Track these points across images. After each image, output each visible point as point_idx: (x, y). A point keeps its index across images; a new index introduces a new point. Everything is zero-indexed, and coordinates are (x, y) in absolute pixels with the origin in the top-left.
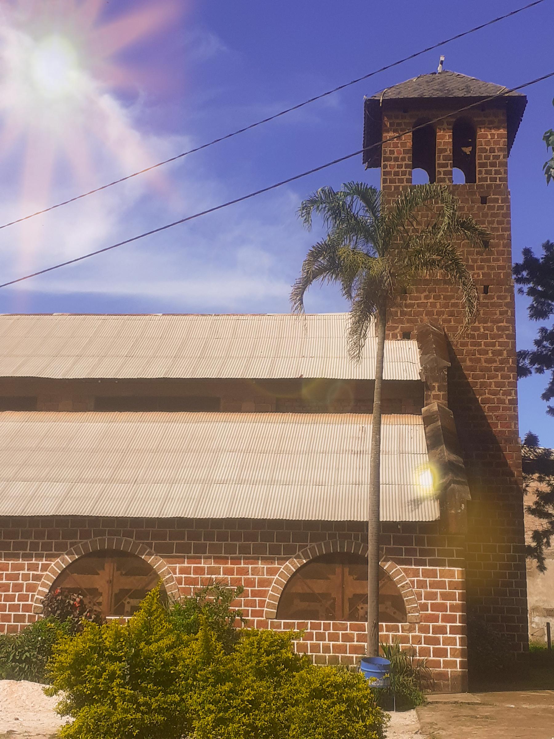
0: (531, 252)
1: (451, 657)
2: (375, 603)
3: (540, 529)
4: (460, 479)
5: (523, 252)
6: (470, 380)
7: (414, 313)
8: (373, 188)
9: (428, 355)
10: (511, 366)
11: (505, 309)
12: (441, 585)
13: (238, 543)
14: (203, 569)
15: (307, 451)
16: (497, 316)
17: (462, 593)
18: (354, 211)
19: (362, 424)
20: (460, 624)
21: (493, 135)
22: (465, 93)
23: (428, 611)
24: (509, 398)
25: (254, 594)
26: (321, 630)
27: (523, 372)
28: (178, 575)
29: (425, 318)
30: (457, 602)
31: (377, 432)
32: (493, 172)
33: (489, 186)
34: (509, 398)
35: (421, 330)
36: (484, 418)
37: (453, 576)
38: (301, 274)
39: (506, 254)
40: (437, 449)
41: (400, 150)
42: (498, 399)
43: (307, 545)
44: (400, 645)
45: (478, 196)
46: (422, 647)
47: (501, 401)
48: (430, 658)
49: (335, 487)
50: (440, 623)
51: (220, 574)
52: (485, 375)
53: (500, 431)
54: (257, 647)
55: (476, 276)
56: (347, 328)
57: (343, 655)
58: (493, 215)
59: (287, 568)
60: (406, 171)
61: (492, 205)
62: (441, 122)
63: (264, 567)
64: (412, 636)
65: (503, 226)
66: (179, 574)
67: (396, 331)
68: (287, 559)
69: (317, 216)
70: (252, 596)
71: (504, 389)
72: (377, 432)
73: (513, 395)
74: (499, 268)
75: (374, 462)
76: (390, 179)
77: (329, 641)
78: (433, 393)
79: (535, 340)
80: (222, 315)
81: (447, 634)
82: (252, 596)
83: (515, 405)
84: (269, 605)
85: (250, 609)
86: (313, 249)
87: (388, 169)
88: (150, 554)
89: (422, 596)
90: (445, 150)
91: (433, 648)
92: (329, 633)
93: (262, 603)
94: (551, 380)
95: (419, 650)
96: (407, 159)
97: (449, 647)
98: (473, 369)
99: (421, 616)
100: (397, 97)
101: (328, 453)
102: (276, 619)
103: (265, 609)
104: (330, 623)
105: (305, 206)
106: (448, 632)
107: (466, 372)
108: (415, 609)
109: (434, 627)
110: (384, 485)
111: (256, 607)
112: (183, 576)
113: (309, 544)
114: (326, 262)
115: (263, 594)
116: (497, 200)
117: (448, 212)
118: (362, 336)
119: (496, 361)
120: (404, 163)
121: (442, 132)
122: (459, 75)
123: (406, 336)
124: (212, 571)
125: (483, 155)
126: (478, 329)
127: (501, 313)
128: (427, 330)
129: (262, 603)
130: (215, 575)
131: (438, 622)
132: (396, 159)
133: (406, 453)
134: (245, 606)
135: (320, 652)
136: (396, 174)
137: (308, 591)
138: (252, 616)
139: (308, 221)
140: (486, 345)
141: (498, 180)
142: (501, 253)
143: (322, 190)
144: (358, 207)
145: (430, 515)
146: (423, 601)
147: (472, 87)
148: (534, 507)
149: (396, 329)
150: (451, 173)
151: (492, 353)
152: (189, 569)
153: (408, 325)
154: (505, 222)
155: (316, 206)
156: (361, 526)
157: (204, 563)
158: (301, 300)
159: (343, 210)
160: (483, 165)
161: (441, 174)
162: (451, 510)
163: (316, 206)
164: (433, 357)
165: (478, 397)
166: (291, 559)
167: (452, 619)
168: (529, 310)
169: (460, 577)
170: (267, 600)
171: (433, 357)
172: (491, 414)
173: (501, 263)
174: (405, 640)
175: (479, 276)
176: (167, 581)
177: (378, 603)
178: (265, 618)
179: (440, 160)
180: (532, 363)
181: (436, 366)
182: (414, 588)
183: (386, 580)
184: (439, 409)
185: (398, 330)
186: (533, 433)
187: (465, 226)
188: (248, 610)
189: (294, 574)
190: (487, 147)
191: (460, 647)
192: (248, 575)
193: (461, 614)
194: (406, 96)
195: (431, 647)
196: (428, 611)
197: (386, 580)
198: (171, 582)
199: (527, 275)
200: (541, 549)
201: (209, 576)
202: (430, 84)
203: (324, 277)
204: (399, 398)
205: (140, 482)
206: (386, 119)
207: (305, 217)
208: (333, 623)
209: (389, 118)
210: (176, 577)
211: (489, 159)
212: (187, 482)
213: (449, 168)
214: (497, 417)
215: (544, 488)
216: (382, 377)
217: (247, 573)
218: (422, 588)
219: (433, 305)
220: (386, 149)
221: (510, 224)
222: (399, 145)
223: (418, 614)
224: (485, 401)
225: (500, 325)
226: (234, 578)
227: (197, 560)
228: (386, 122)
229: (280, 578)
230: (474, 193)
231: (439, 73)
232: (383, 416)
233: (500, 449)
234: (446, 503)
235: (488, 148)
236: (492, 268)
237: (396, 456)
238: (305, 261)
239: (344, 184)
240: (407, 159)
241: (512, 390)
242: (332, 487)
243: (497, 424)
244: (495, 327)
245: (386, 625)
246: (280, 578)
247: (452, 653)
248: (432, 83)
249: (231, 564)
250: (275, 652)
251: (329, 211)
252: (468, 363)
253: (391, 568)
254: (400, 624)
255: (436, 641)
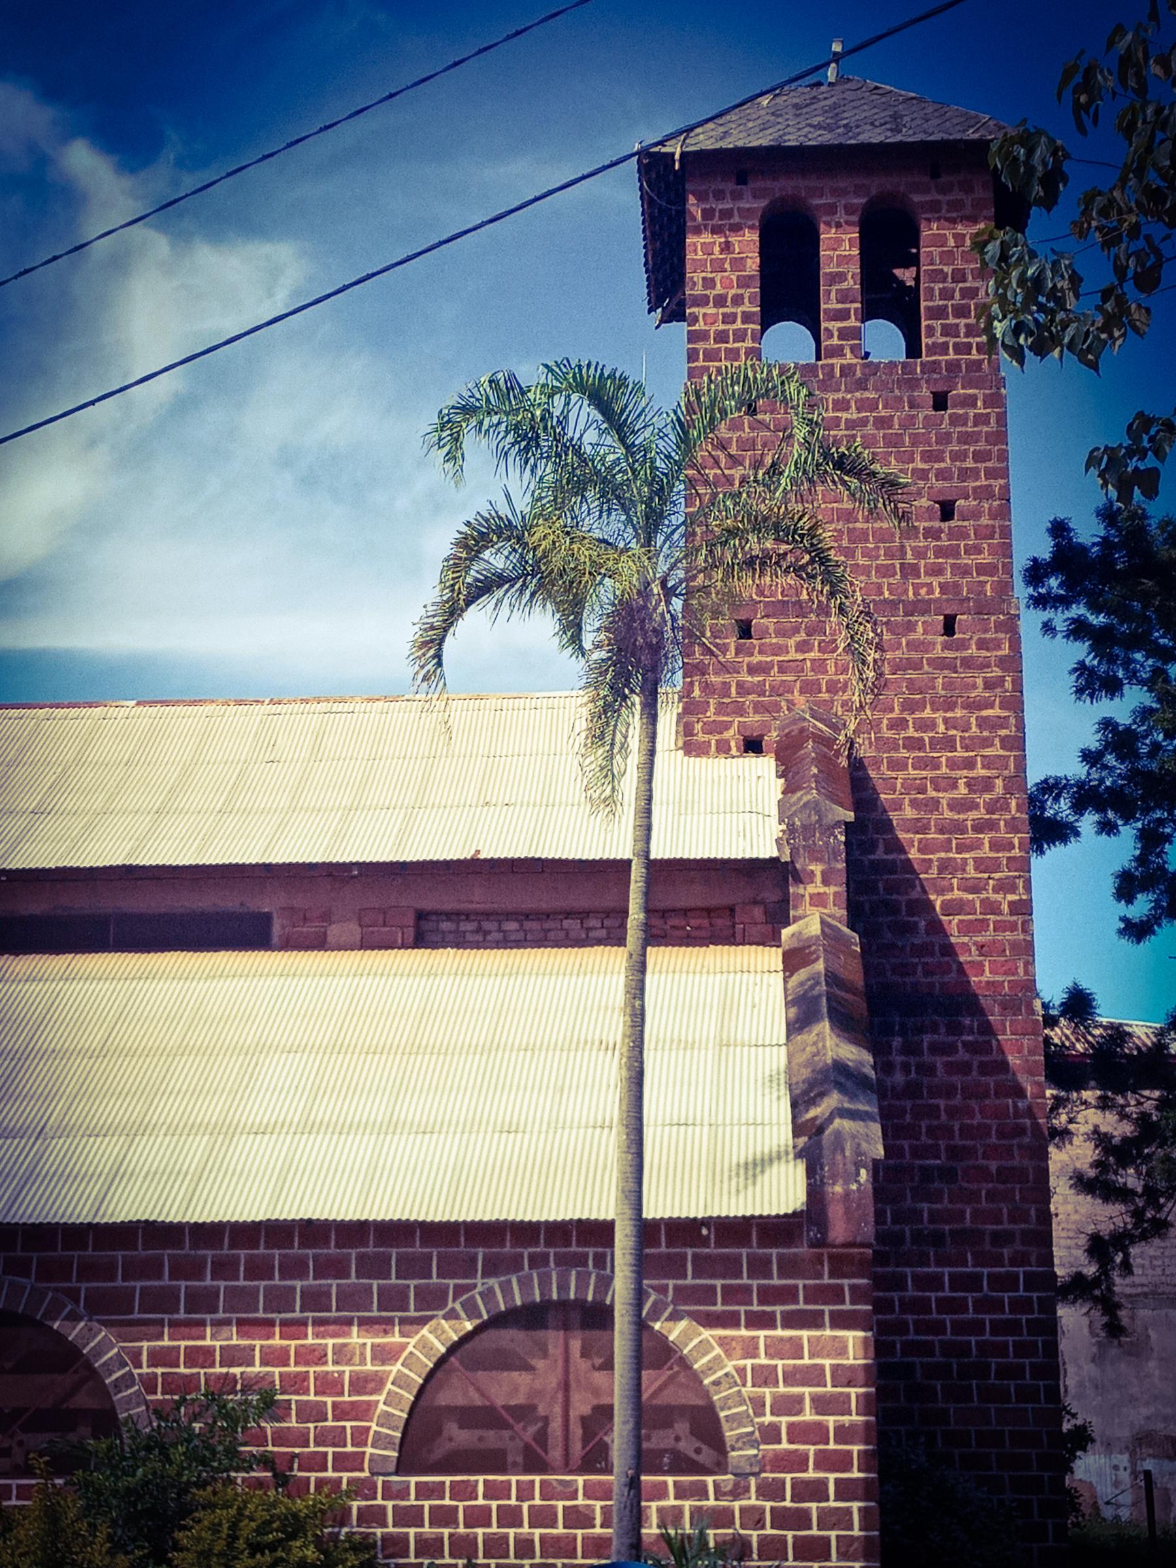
0: (1069, 530)
1: (838, 1560)
2: (630, 1426)
3: (1105, 1229)
7: (772, 688)
9: (799, 794)
10: (1014, 818)
11: (997, 672)
12: (813, 1376)
13: (298, 1284)
14: (209, 1352)
15: (487, 1047)
16: (979, 692)
17: (866, 1395)
19: (598, 971)
20: (861, 1475)
21: (959, 238)
22: (889, 134)
23: (780, 1442)
24: (1010, 897)
25: (341, 1412)
26: (509, 1498)
27: (1048, 832)
28: (145, 1370)
29: (800, 700)
30: (854, 1417)
31: (637, 990)
32: (963, 331)
33: (953, 366)
34: (1010, 897)
35: (787, 731)
36: (949, 950)
37: (842, 1352)
38: (437, 591)
39: (997, 536)
40: (810, 1032)
41: (727, 278)
42: (982, 901)
43: (475, 1286)
44: (710, 1532)
46: (767, 1536)
47: (991, 907)
48: (787, 1564)
49: (551, 1136)
50: (811, 1474)
53: (988, 982)
54: (229, 1536)
56: (577, 730)
58: (965, 438)
59: (424, 1345)
60: (746, 330)
61: (961, 412)
62: (832, 209)
63: (365, 1344)
65: (989, 464)
66: (148, 1367)
67: (727, 735)
68: (423, 1321)
69: (477, 448)
70: (336, 1418)
71: (997, 875)
72: (637, 990)
73: (1021, 890)
74: (982, 569)
75: (629, 1069)
76: (705, 349)
77: (530, 1527)
78: (811, 889)
79: (1082, 751)
80: (289, 702)
81: (827, 1500)
82: (336, 1418)
83: (1027, 917)
84: (379, 1441)
85: (330, 1450)
86: (465, 529)
87: (700, 326)
88: (74, 1317)
89: (764, 1405)
90: (841, 277)
91: (794, 1537)
92: (530, 1507)
93: (360, 1437)
94: (1138, 852)
96: (746, 300)
97: (833, 1534)
99: (764, 1457)
100: (717, 146)
101: (540, 1050)
102: (397, 1473)
103: (369, 1450)
104: (533, 1482)
105: (449, 421)
106: (832, 1496)
107: (902, 835)
108: (748, 1440)
109: (795, 1483)
110: (752, 1128)
112: (159, 1371)
113: (479, 1281)
114: (490, 565)
115: (362, 1411)
116: (971, 402)
119: (976, 807)
120: (739, 310)
121: (833, 230)
122: (876, 88)
125: (937, 287)
126: (930, 725)
127: (989, 685)
128: (802, 730)
129: (360, 1437)
130: (240, 1365)
132: (720, 301)
133: (735, 1046)
134: (317, 1444)
135: (507, 1557)
136: (722, 337)
137: (478, 1401)
138: (335, 1470)
143: (490, 382)
144: (583, 423)
145: (783, 1199)
146: (768, 1418)
147: (906, 119)
149: (727, 729)
150: (856, 334)
151: (968, 785)
152: (174, 1354)
153: (757, 718)
155: (474, 422)
156: (597, 1233)
157: (213, 1337)
158: (438, 656)
159: (545, 428)
161: (832, 336)
163: (474, 422)
164: (809, 797)
165: (932, 897)
166: (433, 1323)
167: (841, 1462)
168: (1074, 677)
169: (861, 1353)
170: (374, 1428)
171: (809, 797)
172: (966, 940)
173: (985, 558)
174: (722, 1518)
175: (931, 591)
176: (118, 1385)
177: (638, 1426)
178: (366, 1474)
179: (829, 303)
180: (1079, 807)
182: (744, 1385)
184: (822, 930)
185: (731, 732)
186: (1084, 984)
188: (326, 1454)
189: (441, 1362)
190: (945, 269)
192: (326, 1363)
193: (862, 1447)
194: (740, 144)
196: (780, 1442)
197: (676, 1368)
198: (128, 1387)
199: (1060, 586)
201: (224, 1370)
203: (499, 602)
204: (711, 902)
205: (51, 1134)
207: (447, 448)
208: (542, 1482)
209: (702, 197)
210: (139, 1375)
211: (952, 298)
213: (852, 322)
215: (1108, 1122)
217: (321, 1359)
218: (765, 1383)
219: (819, 666)
220: (695, 277)
222: (727, 266)
223: (755, 1452)
224: (952, 908)
225: (985, 713)
226: (289, 1374)
227: (195, 1331)
228: (693, 209)
229: (406, 1371)
230: (913, 384)
231: (830, 84)
232: (649, 948)
233: (987, 1029)
235: (948, 269)
236: (965, 571)
239: (546, 366)
242: (543, 1136)
243: (981, 965)
244: (973, 720)
245: (675, 1483)
246: (406, 1371)
247: (843, 1550)
249: (281, 1338)
250: (272, 1547)
252: (909, 813)
253: (686, 1336)
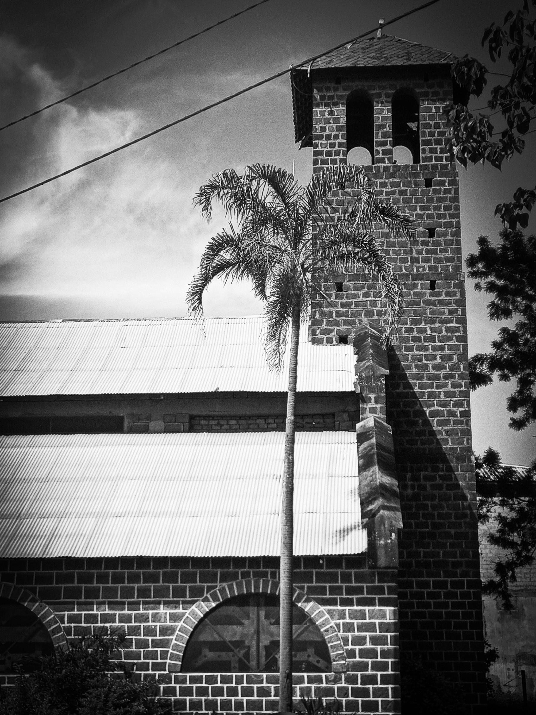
0: (487, 242)
1: (382, 711)
2: (287, 650)
3: (504, 560)
4: (392, 505)
5: (477, 241)
6: (416, 389)
7: (352, 313)
8: (281, 171)
9: (364, 362)
10: (462, 373)
11: (454, 307)
12: (370, 627)
17: (395, 636)
18: (261, 197)
20: (393, 673)
21: (437, 109)
22: (405, 61)
23: (355, 658)
24: (461, 409)
26: (232, 683)
27: (478, 380)
28: (66, 625)
29: (365, 319)
30: (389, 646)
31: (290, 451)
32: (439, 151)
33: (434, 167)
34: (461, 409)
36: (433, 433)
37: (384, 616)
38: (199, 270)
39: (454, 244)
40: (369, 471)
42: (448, 411)
43: (216, 586)
45: (421, 179)
47: (452, 414)
49: (251, 518)
50: (370, 672)
51: (115, 622)
52: (433, 383)
54: (104, 700)
55: (421, 270)
57: (258, 712)
58: (440, 200)
59: (193, 613)
61: (438, 188)
64: (338, 688)
65: (451, 212)
67: (331, 335)
68: (193, 602)
69: (218, 205)
71: (454, 399)
72: (290, 451)
73: (466, 406)
74: (448, 260)
75: (287, 488)
76: (321, 159)
78: (370, 405)
82: (153, 647)
83: (468, 418)
84: (173, 657)
85: (151, 661)
86: (212, 241)
87: (319, 148)
88: (34, 601)
89: (348, 641)
92: (242, 687)
93: (164, 655)
94: (518, 389)
95: (346, 704)
96: (340, 137)
97: (380, 699)
98: (419, 377)
99: (348, 664)
100: (327, 66)
102: (181, 672)
105: (204, 192)
106: (379, 682)
107: (411, 381)
108: (341, 657)
111: (157, 659)
112: (73, 625)
113: (218, 584)
115: (165, 644)
116: (442, 183)
117: (365, 197)
118: (281, 342)
119: (445, 368)
121: (380, 105)
123: (343, 340)
124: (106, 618)
125: (427, 131)
127: (451, 312)
128: (366, 333)
129: (164, 655)
130: (109, 622)
131: (367, 671)
132: (328, 137)
134: (144, 658)
136: (329, 154)
137: (218, 639)
139: (207, 209)
140: (434, 348)
141: (444, 160)
142: (448, 243)
144: (266, 193)
148: (498, 535)
149: (331, 332)
150: (390, 152)
151: (441, 358)
152: (79, 617)
153: (345, 327)
154: (453, 207)
155: (216, 192)
156: (272, 562)
157: (97, 610)
158: (200, 299)
159: (248, 196)
160: (427, 143)
161: (379, 153)
162: (380, 540)
163: (216, 192)
164: (369, 363)
165: (425, 409)
166: (197, 603)
167: (383, 667)
168: (489, 309)
169: (392, 617)
170: (171, 651)
171: (369, 363)
172: (440, 428)
173: (449, 255)
174: (329, 692)
175: (424, 270)
177: (291, 650)
178: (167, 672)
180: (492, 368)
181: (372, 375)
182: (339, 632)
183: (308, 624)
185: (333, 334)
186: (494, 449)
187: (386, 212)
189: (201, 621)
190: (431, 122)
191: (392, 699)
192: (148, 622)
193: (393, 660)
194: (337, 65)
195: (360, 700)
198: (58, 633)
199: (483, 267)
200: (505, 583)
201: (102, 625)
202: (367, 50)
203: (228, 274)
204: (324, 412)
205: (23, 517)
206: (315, 91)
208: (247, 676)
209: (320, 90)
210: (63, 627)
211: (434, 136)
212: (78, 516)
213: (388, 147)
214: (447, 432)
215: (505, 512)
216: (295, 389)
217: (146, 620)
218: (349, 631)
219: (373, 304)
221: (459, 209)
222: (331, 121)
223: (344, 662)
224: (434, 414)
225: (449, 325)
226: (132, 627)
227: (89, 607)
228: (316, 95)
230: (416, 175)
231: (378, 38)
232: (296, 433)
234: (375, 533)
235: (432, 123)
236: (440, 260)
237: (324, 480)
238: (204, 255)
240: (340, 137)
241: (465, 400)
243: (447, 440)
244: (443, 328)
245: (308, 676)
248: (368, 50)
250: (124, 705)
251: (231, 197)
252: (414, 371)
253: (313, 609)
254: (323, 675)
255: (365, 693)
